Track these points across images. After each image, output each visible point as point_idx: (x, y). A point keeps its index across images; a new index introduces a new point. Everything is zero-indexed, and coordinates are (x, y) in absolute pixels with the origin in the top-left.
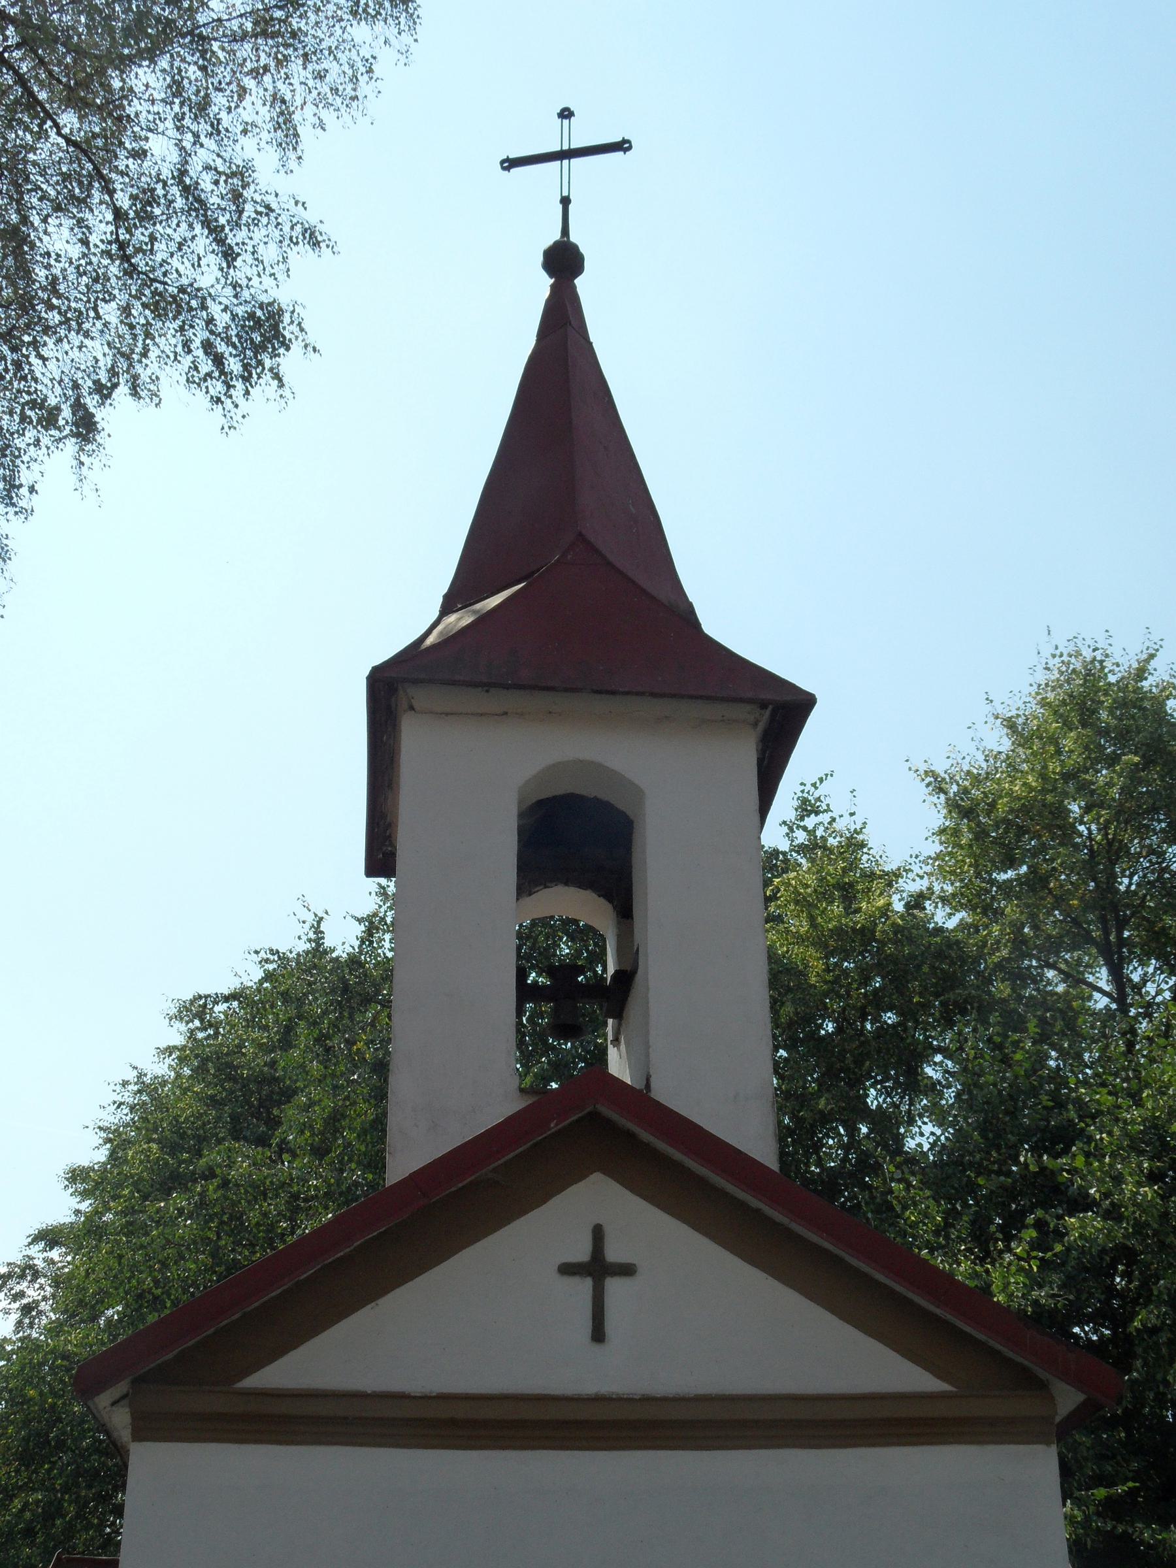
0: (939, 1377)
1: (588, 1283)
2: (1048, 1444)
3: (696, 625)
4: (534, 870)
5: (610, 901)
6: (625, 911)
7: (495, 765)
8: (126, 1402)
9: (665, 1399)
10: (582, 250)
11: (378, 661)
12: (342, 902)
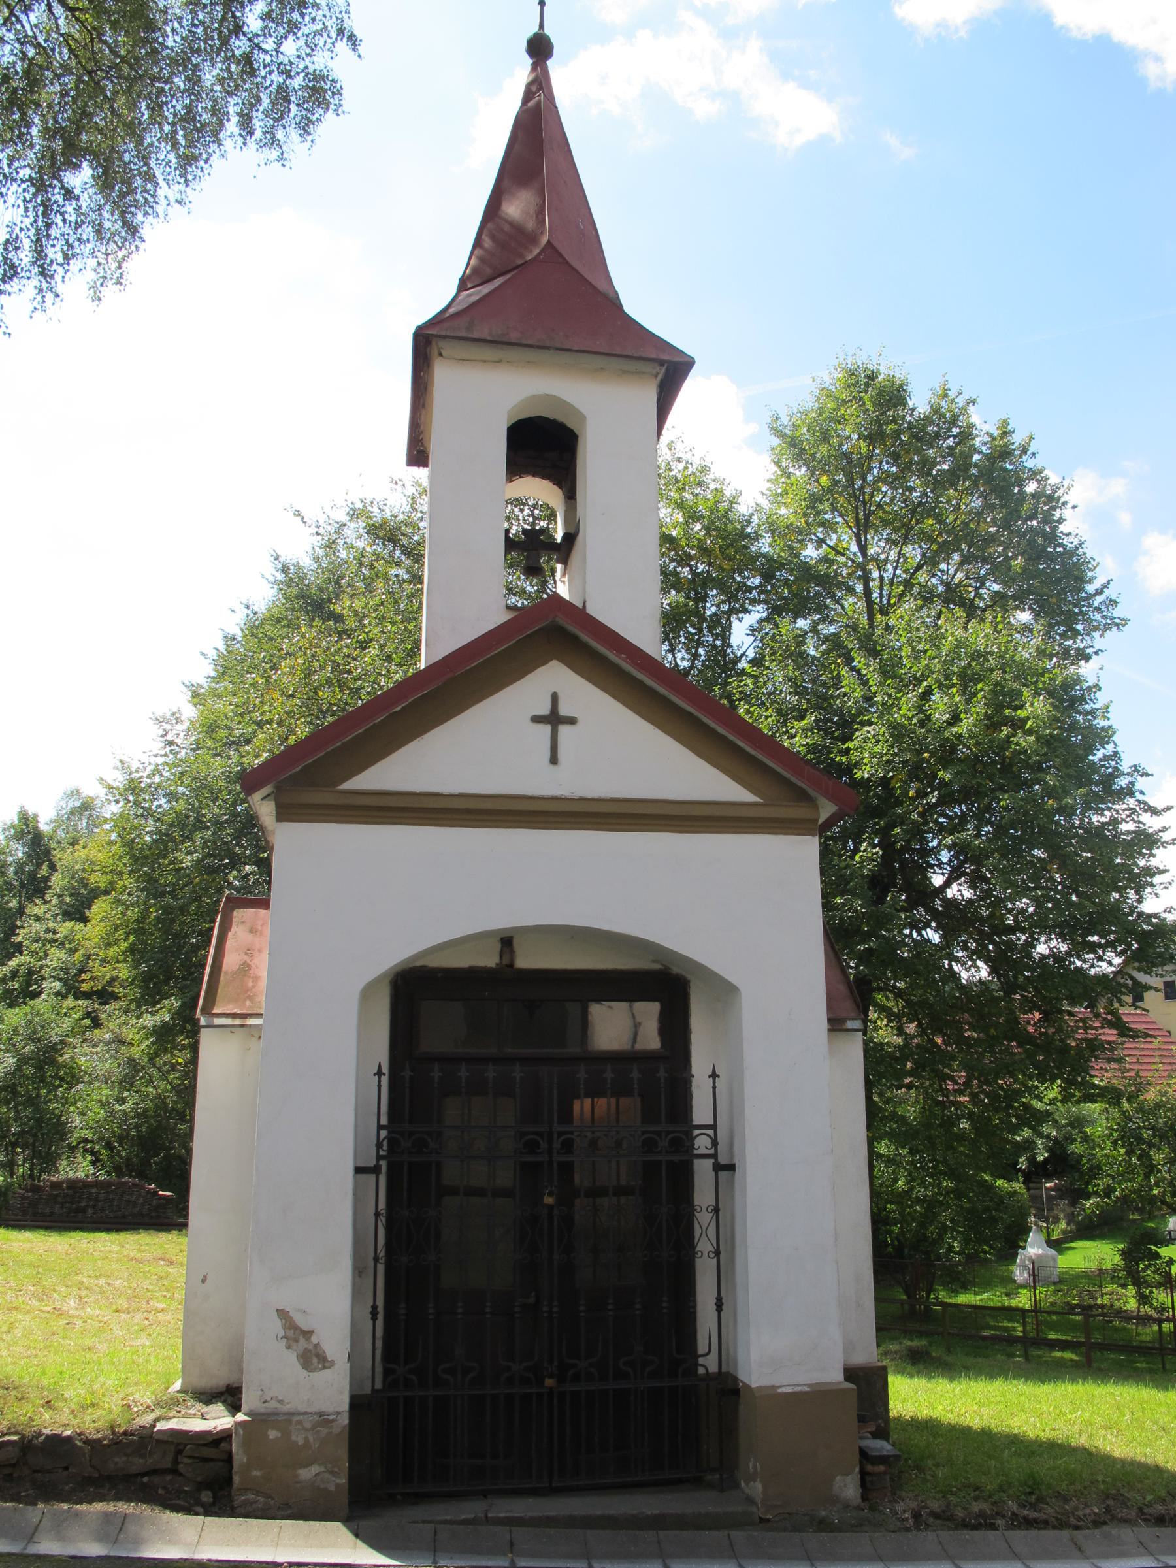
0: (755, 794)
1: (548, 728)
2: (813, 835)
3: (619, 307)
4: (516, 466)
5: (561, 488)
6: (571, 496)
7: (491, 395)
8: (272, 796)
9: (593, 800)
10: (552, 40)
11: (420, 322)
12: (390, 483)
